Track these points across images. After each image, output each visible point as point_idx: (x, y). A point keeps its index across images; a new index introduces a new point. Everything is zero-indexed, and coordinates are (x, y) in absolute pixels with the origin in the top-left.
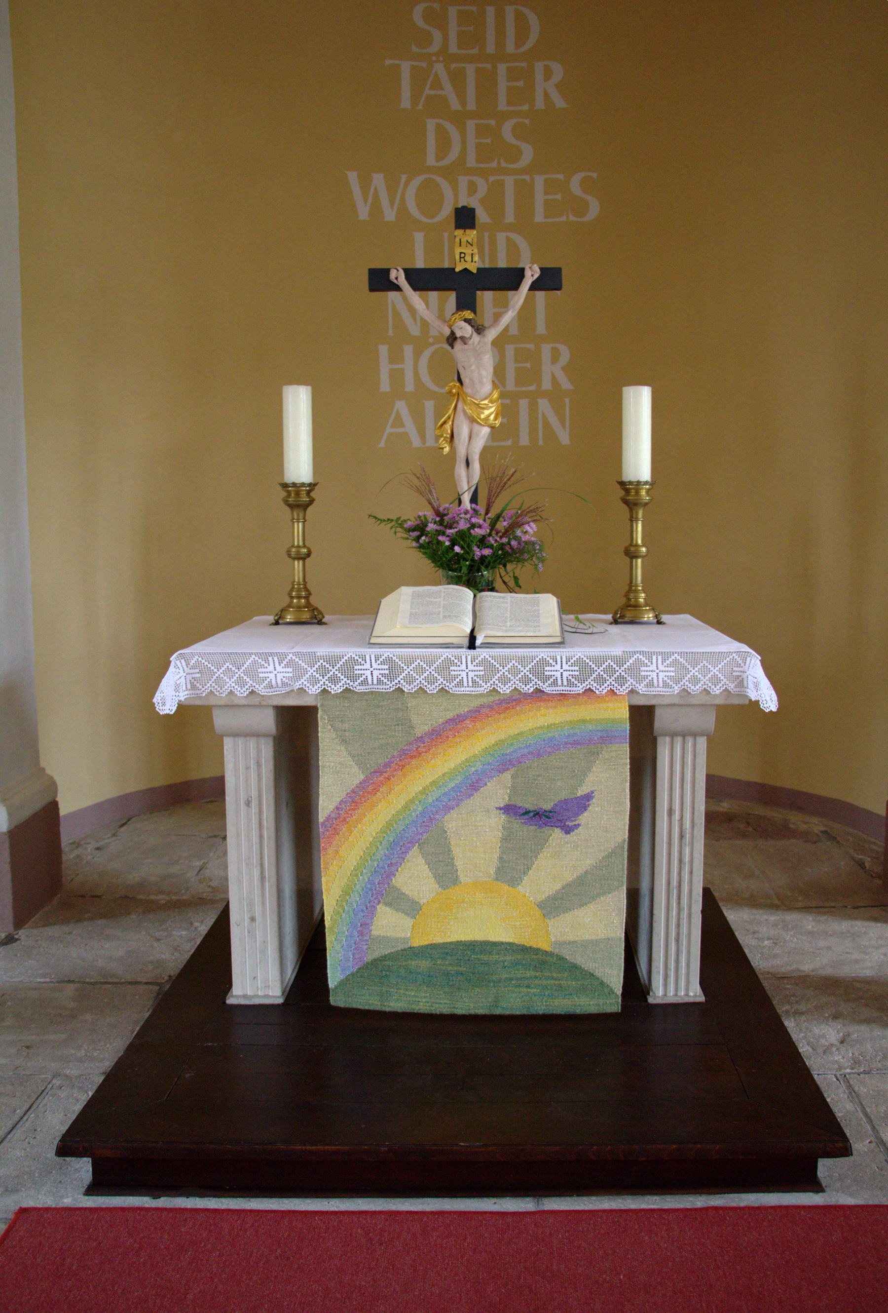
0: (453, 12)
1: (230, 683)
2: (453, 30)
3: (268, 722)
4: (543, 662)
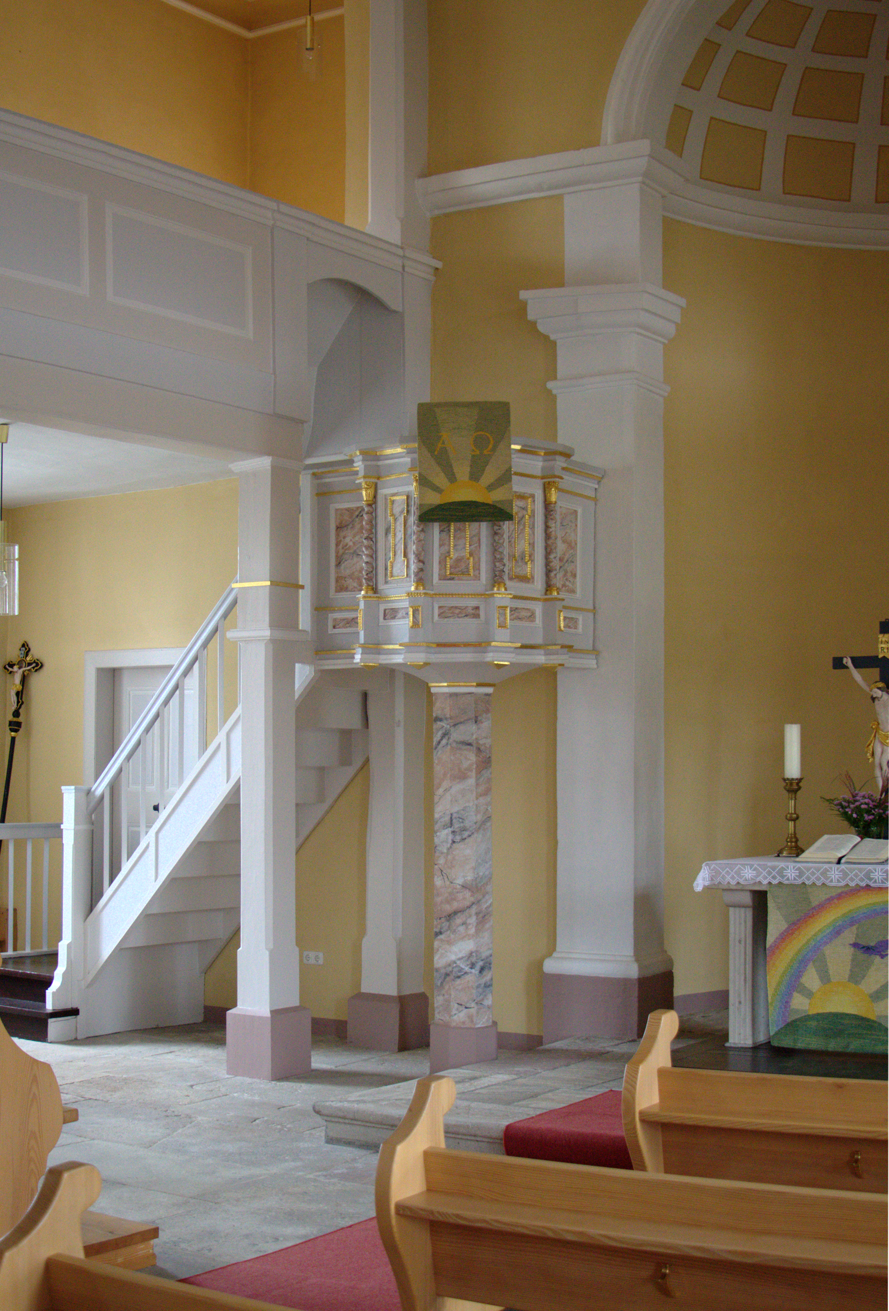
1: (728, 878)
3: (747, 899)
4: (870, 871)
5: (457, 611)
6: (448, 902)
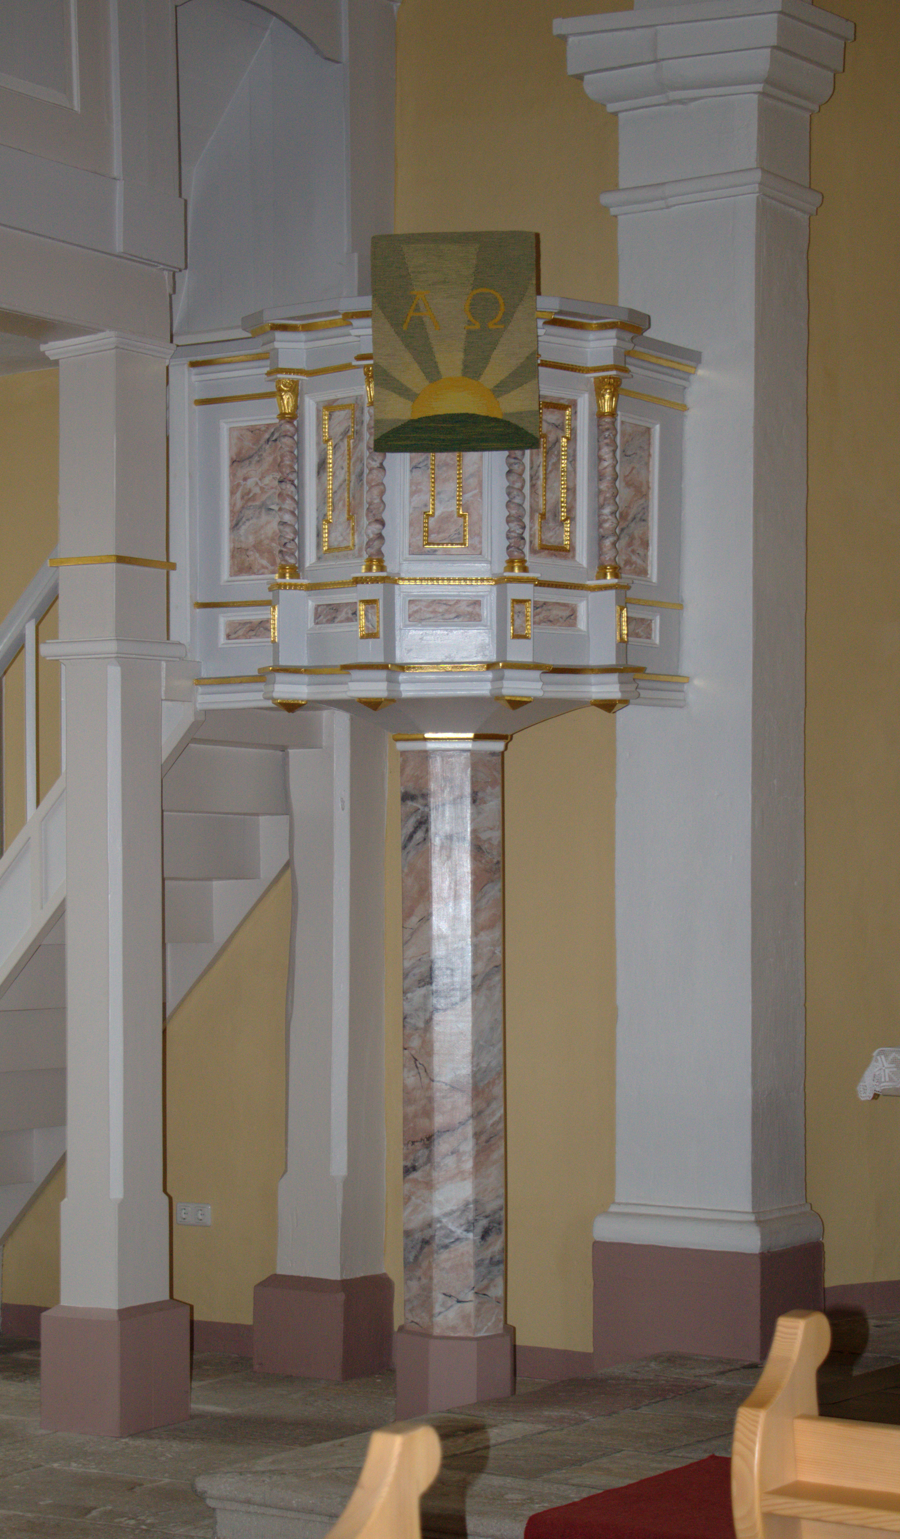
5: (441, 609)
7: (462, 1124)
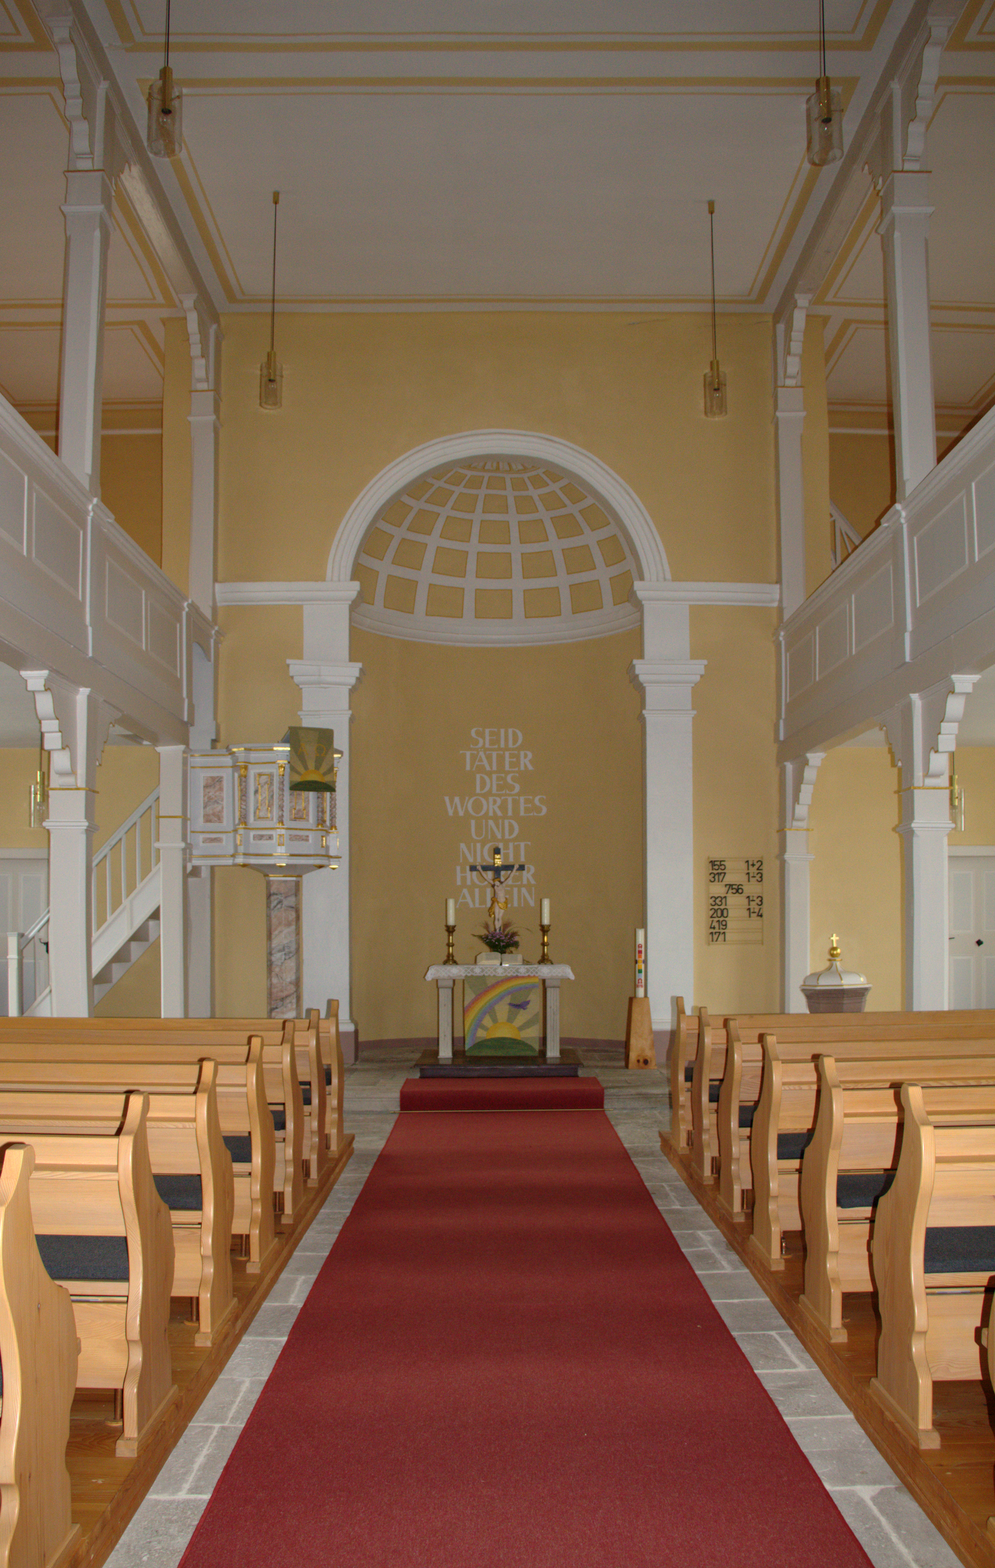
0: (487, 731)
2: (487, 738)
4: (518, 969)
5: (298, 837)
6: (282, 991)
7: (293, 994)
